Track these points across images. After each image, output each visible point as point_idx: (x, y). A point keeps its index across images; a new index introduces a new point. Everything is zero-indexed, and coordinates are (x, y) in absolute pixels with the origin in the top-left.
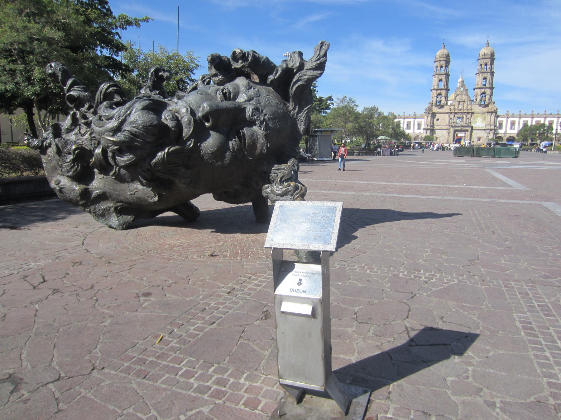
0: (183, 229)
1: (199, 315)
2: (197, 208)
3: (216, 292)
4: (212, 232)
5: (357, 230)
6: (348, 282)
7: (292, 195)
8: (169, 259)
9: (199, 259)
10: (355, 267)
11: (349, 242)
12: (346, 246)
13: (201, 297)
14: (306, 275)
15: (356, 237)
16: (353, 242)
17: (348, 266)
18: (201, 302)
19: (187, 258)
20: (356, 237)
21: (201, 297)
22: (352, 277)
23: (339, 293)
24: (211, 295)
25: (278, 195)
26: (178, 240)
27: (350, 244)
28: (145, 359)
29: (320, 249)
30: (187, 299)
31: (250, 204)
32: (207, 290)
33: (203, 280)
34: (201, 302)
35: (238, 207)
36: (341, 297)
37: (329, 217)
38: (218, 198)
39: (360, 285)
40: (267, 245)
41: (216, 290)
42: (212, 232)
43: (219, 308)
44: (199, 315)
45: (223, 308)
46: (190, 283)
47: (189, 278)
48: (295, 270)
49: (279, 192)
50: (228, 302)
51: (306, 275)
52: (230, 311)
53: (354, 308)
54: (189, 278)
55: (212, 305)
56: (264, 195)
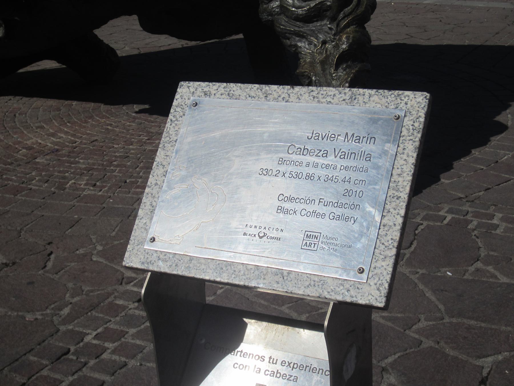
0: (74, 103)
1: (45, 372)
2: (112, 51)
3: (109, 295)
4: (140, 112)
5: (506, 107)
6: (472, 269)
7: (333, 19)
8: (16, 191)
9: (90, 191)
10: (495, 221)
11: (484, 142)
12: (476, 153)
13: (66, 311)
14: (283, 370)
15: (502, 128)
16: (495, 140)
17: (477, 215)
18: (63, 328)
19: (61, 187)
20: (502, 128)
21: (66, 311)
22: (483, 253)
23: (441, 307)
24: (93, 307)
25: (298, 18)
26: (53, 135)
27: (487, 149)
28: (81, 332)
29: (326, 294)
30: (29, 317)
31: (241, 36)
32: (86, 288)
33: (84, 255)
34: (63, 328)
35: (204, 44)
36: (447, 320)
37: (369, 158)
38: (150, 26)
39: (504, 279)
40: (133, 259)
41: (110, 289)
42: (140, 112)
43: (105, 350)
44: (45, 372)
45: (114, 352)
46: (50, 264)
47: (49, 249)
48: (243, 347)
49: (300, 11)
50: (132, 331)
51: (283, 370)
52: (132, 363)
53: (479, 362)
54: (49, 249)
55: (88, 339)
56: (265, 17)
